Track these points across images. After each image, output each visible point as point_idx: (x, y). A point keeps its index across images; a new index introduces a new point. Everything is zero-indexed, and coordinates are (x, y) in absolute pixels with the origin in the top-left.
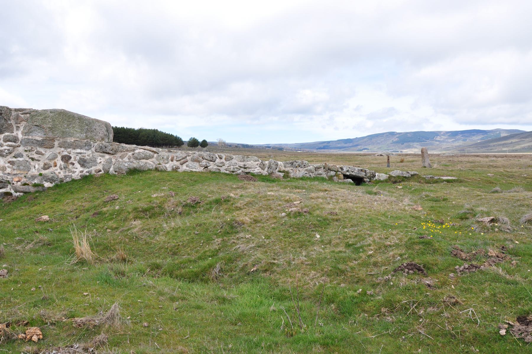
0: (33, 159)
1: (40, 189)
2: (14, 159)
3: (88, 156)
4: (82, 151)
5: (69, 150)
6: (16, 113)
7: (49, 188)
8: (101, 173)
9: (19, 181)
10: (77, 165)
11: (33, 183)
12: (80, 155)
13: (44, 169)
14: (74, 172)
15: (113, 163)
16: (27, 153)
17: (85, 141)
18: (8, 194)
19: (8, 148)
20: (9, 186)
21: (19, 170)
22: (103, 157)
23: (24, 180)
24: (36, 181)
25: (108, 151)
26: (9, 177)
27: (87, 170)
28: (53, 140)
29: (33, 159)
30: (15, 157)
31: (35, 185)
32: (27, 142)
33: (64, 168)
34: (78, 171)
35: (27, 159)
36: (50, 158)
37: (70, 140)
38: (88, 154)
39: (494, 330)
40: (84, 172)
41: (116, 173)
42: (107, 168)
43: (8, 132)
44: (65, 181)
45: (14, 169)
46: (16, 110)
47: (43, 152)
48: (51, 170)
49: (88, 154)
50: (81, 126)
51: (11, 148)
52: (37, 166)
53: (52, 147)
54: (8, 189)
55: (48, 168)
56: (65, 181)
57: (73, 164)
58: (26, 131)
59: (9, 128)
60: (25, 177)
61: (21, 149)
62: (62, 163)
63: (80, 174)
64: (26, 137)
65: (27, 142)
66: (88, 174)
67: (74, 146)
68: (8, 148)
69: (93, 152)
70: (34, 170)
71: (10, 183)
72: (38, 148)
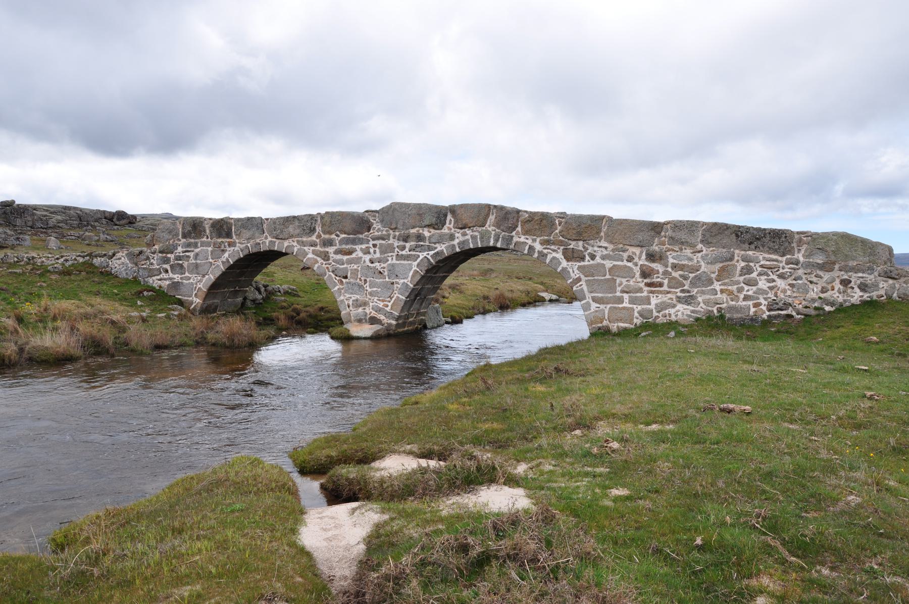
0: (811, 282)
1: (821, 312)
2: (794, 282)
3: (870, 280)
4: (864, 275)
5: (850, 274)
6: (798, 236)
7: (830, 312)
8: (883, 298)
9: (800, 304)
10: (857, 290)
11: (814, 306)
12: (861, 279)
13: (822, 293)
14: (853, 297)
15: (897, 288)
16: (806, 276)
17: (868, 265)
18: (790, 316)
19: (790, 270)
20: (790, 308)
21: (799, 292)
22: (886, 281)
23: (804, 303)
24: (816, 305)
25: (893, 276)
26: (790, 299)
27: (868, 295)
28: (834, 263)
29: (811, 282)
30: (795, 279)
31: (816, 309)
32: (807, 265)
33: (843, 292)
34: (856, 296)
35: (806, 282)
36: (829, 281)
37: (852, 263)
38: (870, 278)
39: (613, 434)
40: (864, 297)
41: (900, 299)
42: (890, 293)
43: (790, 255)
44: (844, 306)
45: (794, 292)
46: (798, 233)
47: (823, 276)
48: (830, 293)
49: (870, 278)
50: (864, 250)
51: (792, 271)
52: (815, 289)
53: (832, 270)
54: (790, 311)
55: (826, 292)
56: (844, 306)
57: (853, 288)
58: (807, 254)
59: (791, 252)
60: (804, 299)
61: (800, 272)
62: (841, 287)
63: (860, 299)
64: (807, 260)
65: (807, 265)
66: (869, 299)
67: (855, 270)
68: (790, 270)
69: (875, 277)
70: (812, 293)
71: (791, 305)
72: (818, 271)
